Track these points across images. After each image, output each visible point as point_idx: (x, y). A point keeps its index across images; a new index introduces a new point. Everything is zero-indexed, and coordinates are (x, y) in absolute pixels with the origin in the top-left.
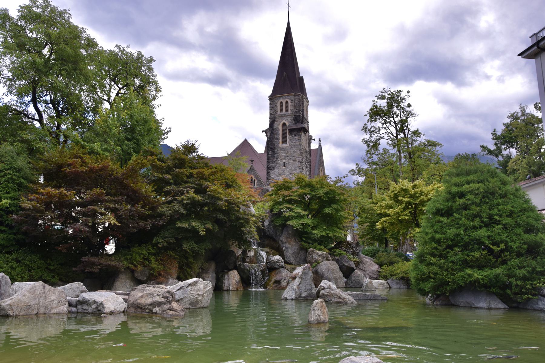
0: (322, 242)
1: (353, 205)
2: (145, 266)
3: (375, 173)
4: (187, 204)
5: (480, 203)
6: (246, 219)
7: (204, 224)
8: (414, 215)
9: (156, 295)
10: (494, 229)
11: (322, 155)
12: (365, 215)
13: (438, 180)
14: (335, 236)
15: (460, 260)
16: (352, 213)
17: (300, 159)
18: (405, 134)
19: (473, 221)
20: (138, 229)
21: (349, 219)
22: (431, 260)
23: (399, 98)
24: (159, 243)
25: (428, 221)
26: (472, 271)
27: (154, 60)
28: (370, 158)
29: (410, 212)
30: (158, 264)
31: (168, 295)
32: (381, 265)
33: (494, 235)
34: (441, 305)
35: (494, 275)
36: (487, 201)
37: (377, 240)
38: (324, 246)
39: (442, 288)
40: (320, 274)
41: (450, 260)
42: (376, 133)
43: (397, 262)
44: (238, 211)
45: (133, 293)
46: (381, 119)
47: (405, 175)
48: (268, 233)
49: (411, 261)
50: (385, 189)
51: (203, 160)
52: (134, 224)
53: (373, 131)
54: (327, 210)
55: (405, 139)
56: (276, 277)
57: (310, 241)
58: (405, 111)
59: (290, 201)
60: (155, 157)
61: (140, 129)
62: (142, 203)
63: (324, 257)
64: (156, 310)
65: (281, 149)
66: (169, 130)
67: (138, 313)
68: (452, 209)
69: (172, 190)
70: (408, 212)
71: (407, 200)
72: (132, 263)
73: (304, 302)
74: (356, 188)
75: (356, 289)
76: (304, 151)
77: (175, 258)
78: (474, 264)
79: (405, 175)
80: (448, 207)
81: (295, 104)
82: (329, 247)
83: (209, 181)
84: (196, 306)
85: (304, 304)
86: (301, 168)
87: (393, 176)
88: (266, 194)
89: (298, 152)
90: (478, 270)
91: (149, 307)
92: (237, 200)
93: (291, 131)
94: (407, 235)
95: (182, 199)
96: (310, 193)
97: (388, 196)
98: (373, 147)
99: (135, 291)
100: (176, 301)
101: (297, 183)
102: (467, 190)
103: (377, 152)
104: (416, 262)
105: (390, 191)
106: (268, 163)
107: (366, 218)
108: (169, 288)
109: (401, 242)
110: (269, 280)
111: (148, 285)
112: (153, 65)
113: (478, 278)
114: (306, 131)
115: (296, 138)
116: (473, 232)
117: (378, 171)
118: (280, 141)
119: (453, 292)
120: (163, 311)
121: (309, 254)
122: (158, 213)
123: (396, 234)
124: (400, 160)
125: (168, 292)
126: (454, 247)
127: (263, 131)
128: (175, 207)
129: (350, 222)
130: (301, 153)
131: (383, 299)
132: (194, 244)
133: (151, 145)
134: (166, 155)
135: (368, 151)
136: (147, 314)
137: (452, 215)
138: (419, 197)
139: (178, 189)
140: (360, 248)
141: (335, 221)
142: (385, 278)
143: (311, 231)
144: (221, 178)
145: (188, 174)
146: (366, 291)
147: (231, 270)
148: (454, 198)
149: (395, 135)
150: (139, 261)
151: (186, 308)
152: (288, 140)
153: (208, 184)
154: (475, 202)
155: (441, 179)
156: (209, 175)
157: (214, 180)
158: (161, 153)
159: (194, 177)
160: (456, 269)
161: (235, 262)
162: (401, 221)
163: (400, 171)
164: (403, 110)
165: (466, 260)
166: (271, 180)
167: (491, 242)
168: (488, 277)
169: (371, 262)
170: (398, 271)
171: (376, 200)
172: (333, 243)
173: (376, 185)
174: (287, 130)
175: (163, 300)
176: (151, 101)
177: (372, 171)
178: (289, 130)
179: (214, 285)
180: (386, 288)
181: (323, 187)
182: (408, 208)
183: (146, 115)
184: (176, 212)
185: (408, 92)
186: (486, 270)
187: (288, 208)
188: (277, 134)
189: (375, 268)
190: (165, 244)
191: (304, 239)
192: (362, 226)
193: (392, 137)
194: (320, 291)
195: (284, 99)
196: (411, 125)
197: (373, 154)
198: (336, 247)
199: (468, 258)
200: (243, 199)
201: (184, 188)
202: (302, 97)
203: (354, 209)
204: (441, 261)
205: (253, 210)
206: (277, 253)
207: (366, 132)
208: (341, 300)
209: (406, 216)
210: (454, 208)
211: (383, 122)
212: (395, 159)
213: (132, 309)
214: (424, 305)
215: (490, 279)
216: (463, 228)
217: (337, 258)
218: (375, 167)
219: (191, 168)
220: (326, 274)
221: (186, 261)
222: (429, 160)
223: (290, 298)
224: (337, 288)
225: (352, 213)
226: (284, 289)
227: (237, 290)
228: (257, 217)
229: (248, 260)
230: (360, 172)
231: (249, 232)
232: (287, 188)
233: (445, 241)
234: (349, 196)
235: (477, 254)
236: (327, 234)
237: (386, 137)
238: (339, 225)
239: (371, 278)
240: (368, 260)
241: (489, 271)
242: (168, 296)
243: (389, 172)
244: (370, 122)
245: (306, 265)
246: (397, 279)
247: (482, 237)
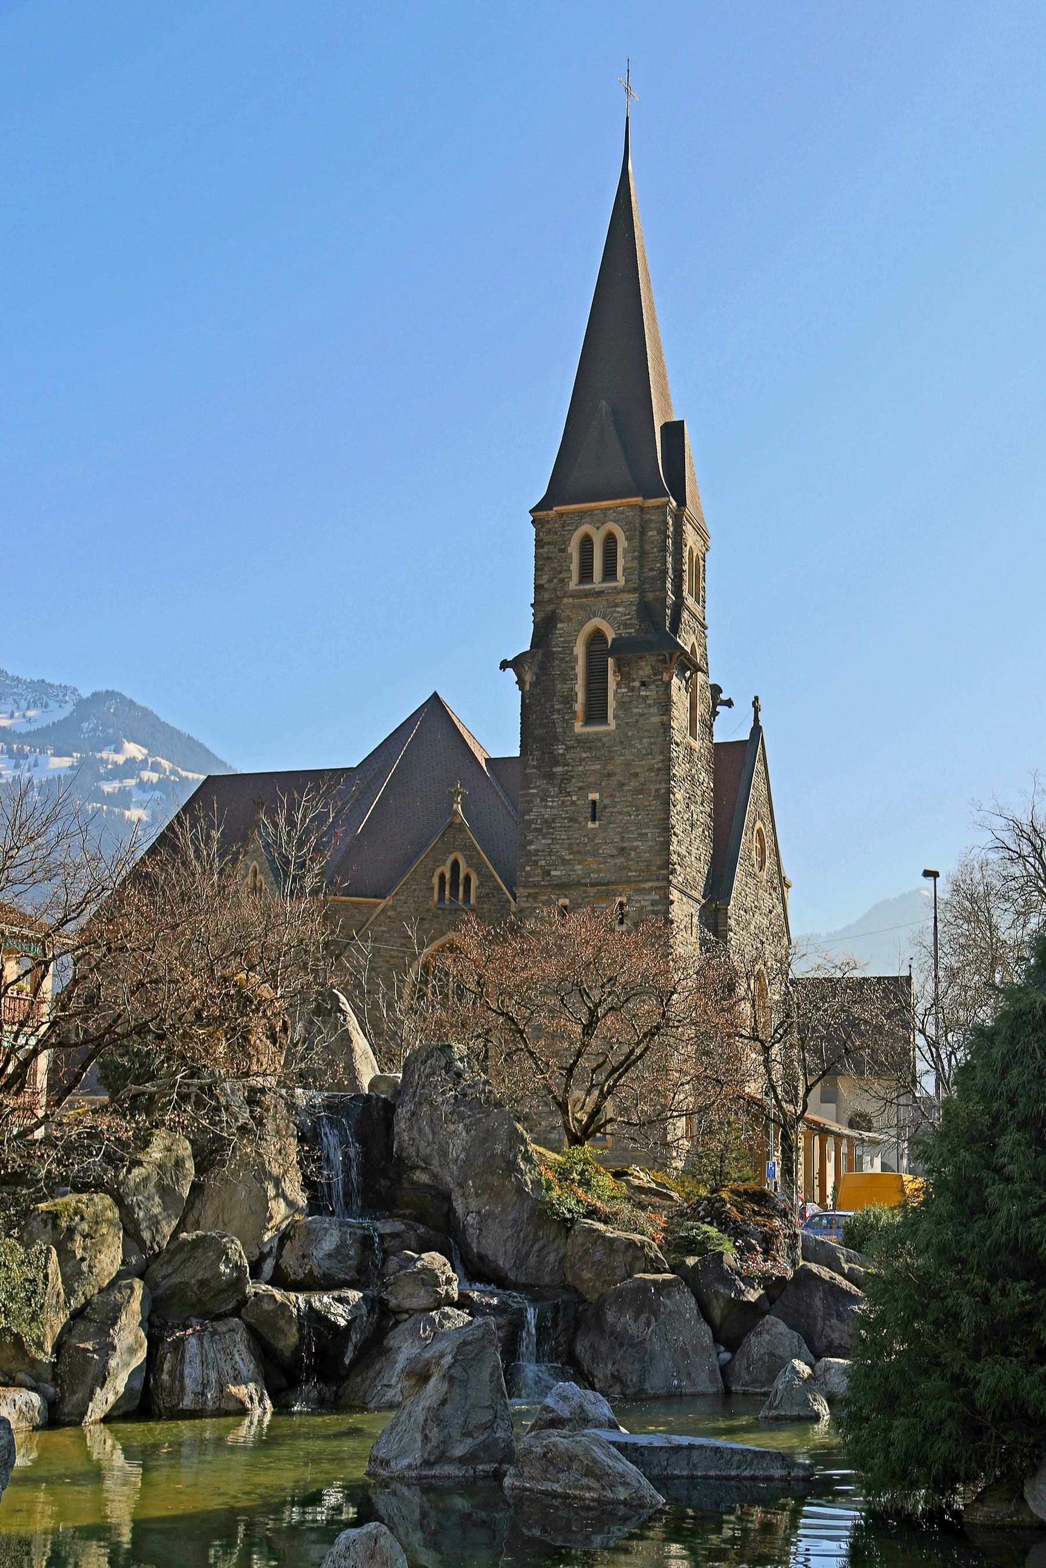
127: (504, 665)
195: (599, 524)
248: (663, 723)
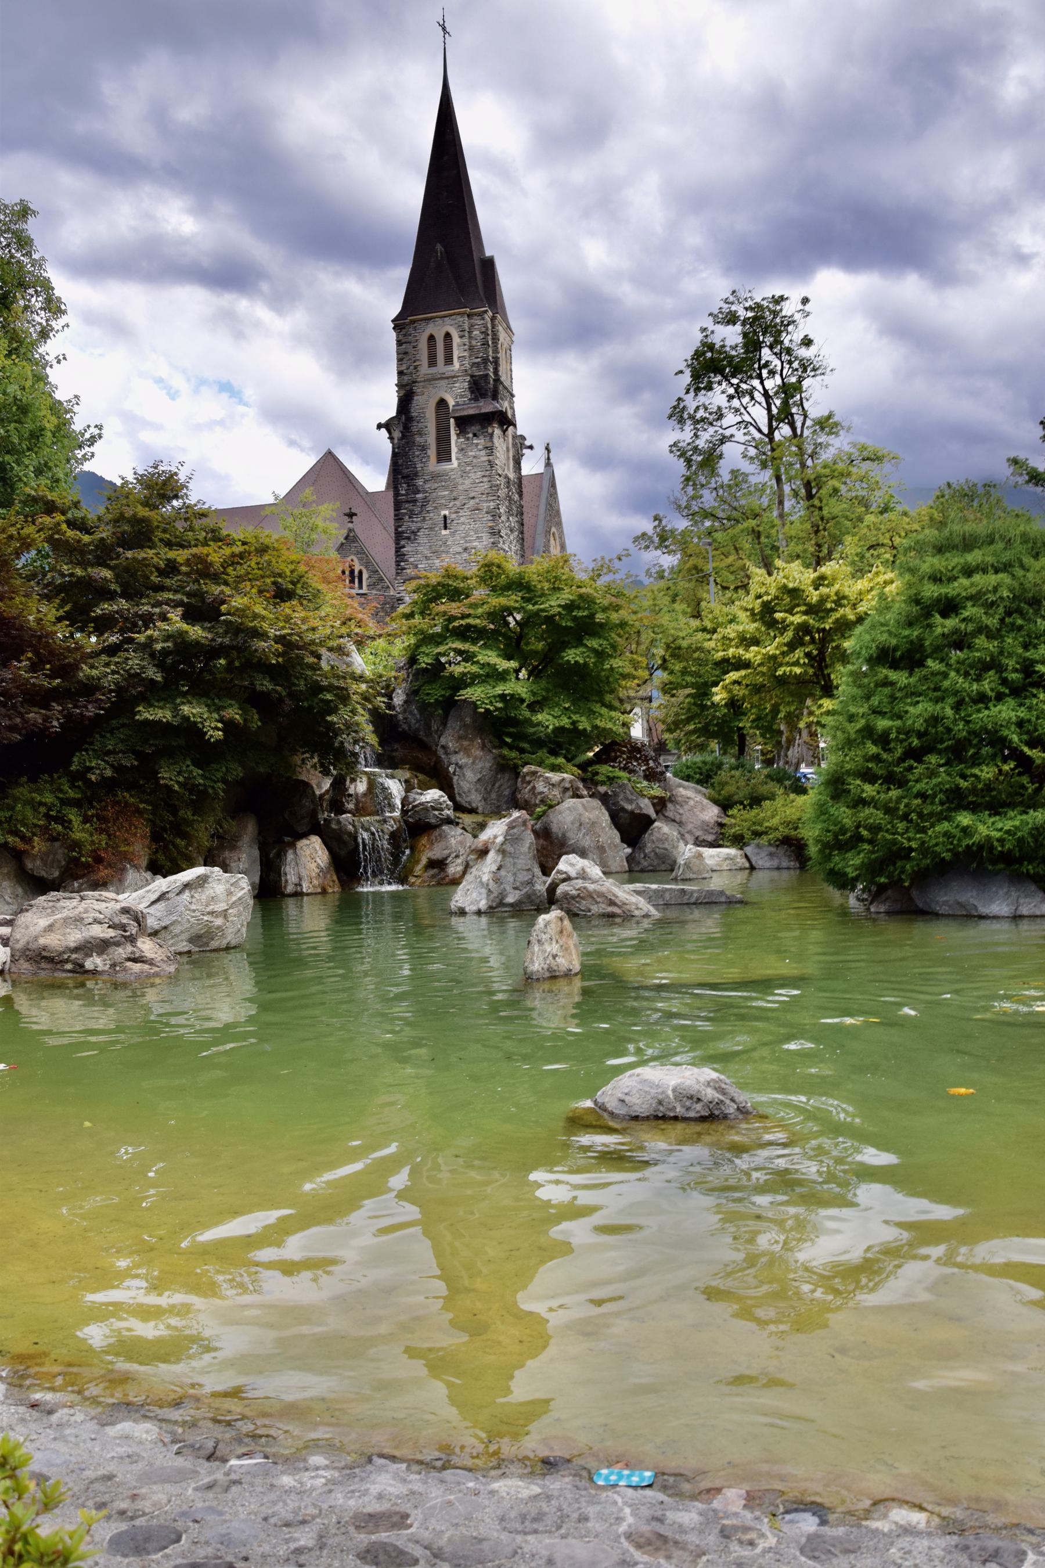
0: (559, 745)
1: (646, 637)
2: (53, 839)
3: (710, 544)
4: (165, 652)
5: (999, 630)
6: (338, 688)
7: (218, 709)
8: (820, 663)
9: (91, 920)
10: (1035, 701)
11: (556, 493)
12: (682, 665)
13: (887, 561)
14: (596, 727)
15: (941, 790)
16: (643, 661)
17: (492, 505)
18: (793, 428)
19: (978, 679)
20: (23, 732)
21: (634, 678)
22: (863, 791)
23: (778, 320)
24: (90, 769)
25: (854, 682)
26: (974, 817)
27: (34, 212)
28: (693, 498)
29: (808, 655)
30: (91, 829)
31: (124, 919)
32: (725, 805)
33: (1033, 719)
34: (888, 913)
35: (1032, 829)
36: (1020, 622)
37: (713, 735)
38: (565, 758)
39: (891, 868)
40: (557, 838)
41: (915, 790)
42: (711, 424)
43: (772, 797)
44: (315, 668)
45: (24, 919)
46: (724, 384)
47: (795, 548)
48: (405, 727)
49: (810, 792)
50: (736, 588)
51: (204, 521)
52: (10, 719)
53: (703, 420)
54: (573, 655)
55: (795, 441)
56: (432, 850)
57: (526, 746)
58: (796, 358)
59: (464, 633)
60: (59, 517)
61: (7, 431)
62: (30, 655)
63: (566, 790)
64: (95, 962)
65: (436, 477)
66: (96, 431)
67: (43, 974)
68: (922, 646)
69: (117, 612)
70: (802, 655)
71: (798, 619)
72: (16, 833)
73: (513, 917)
74: (655, 588)
75: (658, 874)
76: (502, 481)
77: (139, 812)
78: (979, 800)
79: (795, 548)
80: (912, 642)
81: (474, 343)
82: (581, 758)
83: (226, 584)
84: (207, 944)
85: (513, 924)
86: (495, 533)
87: (762, 551)
88: (393, 615)
89: (486, 485)
90: (990, 816)
91: (74, 956)
92: (310, 636)
93: (464, 423)
94: (799, 717)
95: (150, 637)
96: (523, 608)
97: (747, 610)
98: (702, 465)
99: (28, 914)
100: (150, 935)
101: (483, 580)
102: (964, 594)
103: (713, 481)
104: (824, 798)
105: (753, 593)
106: (398, 519)
107: (684, 672)
108: (129, 898)
109: (784, 739)
110: (414, 859)
111: (67, 895)
112: (32, 227)
113: (988, 838)
114: (505, 421)
115: (477, 444)
116: (979, 711)
117: (719, 536)
118: (432, 452)
119: (924, 878)
120: (113, 965)
121: (523, 782)
122: (80, 682)
123: (769, 718)
124: (781, 503)
125: (125, 911)
126: (926, 754)
127: (379, 426)
128: (130, 662)
129: (639, 685)
130: (494, 488)
131: (731, 902)
132: (192, 767)
133: (44, 481)
134: (93, 510)
135: (688, 479)
136: (70, 975)
137: (921, 664)
138: (832, 610)
139: (136, 609)
140: (670, 758)
141: (595, 687)
142: (738, 841)
143: (527, 714)
144: (261, 572)
145: (162, 565)
146: (685, 880)
147: (305, 835)
148: (928, 615)
149: (766, 430)
150: (36, 826)
151: (180, 954)
152: (454, 449)
153: (222, 592)
154: (987, 626)
155: (895, 556)
156: (225, 565)
157: (240, 579)
158: (76, 505)
159: (179, 573)
160: (931, 815)
161: (314, 814)
162: (782, 681)
163: (781, 536)
164: (790, 355)
165: (958, 788)
166: (410, 572)
167: (1025, 737)
168: (1015, 834)
169: (699, 798)
170: (775, 822)
171: (712, 621)
172: (590, 749)
173: (712, 579)
174: (452, 421)
175: (111, 933)
176: (34, 344)
177: (699, 538)
178: (457, 419)
179: (257, 880)
180: (741, 869)
181: (559, 589)
182: (803, 644)
183: (23, 389)
184: (134, 677)
185: (805, 301)
186: (1011, 814)
187: (459, 652)
188: (420, 433)
189: (711, 814)
190: (109, 773)
191: (508, 740)
192: (673, 696)
193: (757, 435)
194: (557, 885)
196: (811, 401)
197: (702, 486)
198: (599, 759)
199: (964, 784)
200: (328, 631)
201: (153, 606)
202: (493, 319)
203: (648, 649)
204: (891, 793)
205: (359, 662)
206: (433, 782)
207: (681, 421)
209: (796, 665)
210: (927, 643)
211: (731, 391)
212: (765, 501)
213: (25, 966)
214: (844, 912)
215: (1021, 840)
216: (951, 700)
217: (602, 789)
218: (708, 523)
219: (169, 544)
220: (574, 837)
221: (171, 818)
222: (865, 503)
223: (474, 908)
224: (604, 873)
225: (643, 661)
226: (456, 882)
227: (324, 892)
228: (372, 681)
229: (351, 806)
230: (666, 540)
231: (351, 727)
232: (455, 594)
233: (902, 736)
234: (635, 613)
235: (986, 773)
236: (574, 723)
237: (740, 436)
238: (608, 698)
239: (699, 842)
240: (689, 793)
241: (1019, 817)
242: (125, 921)
243: (750, 538)
244: (692, 394)
245: (516, 814)
246: (770, 845)
247: (1001, 726)
248: (490, 461)
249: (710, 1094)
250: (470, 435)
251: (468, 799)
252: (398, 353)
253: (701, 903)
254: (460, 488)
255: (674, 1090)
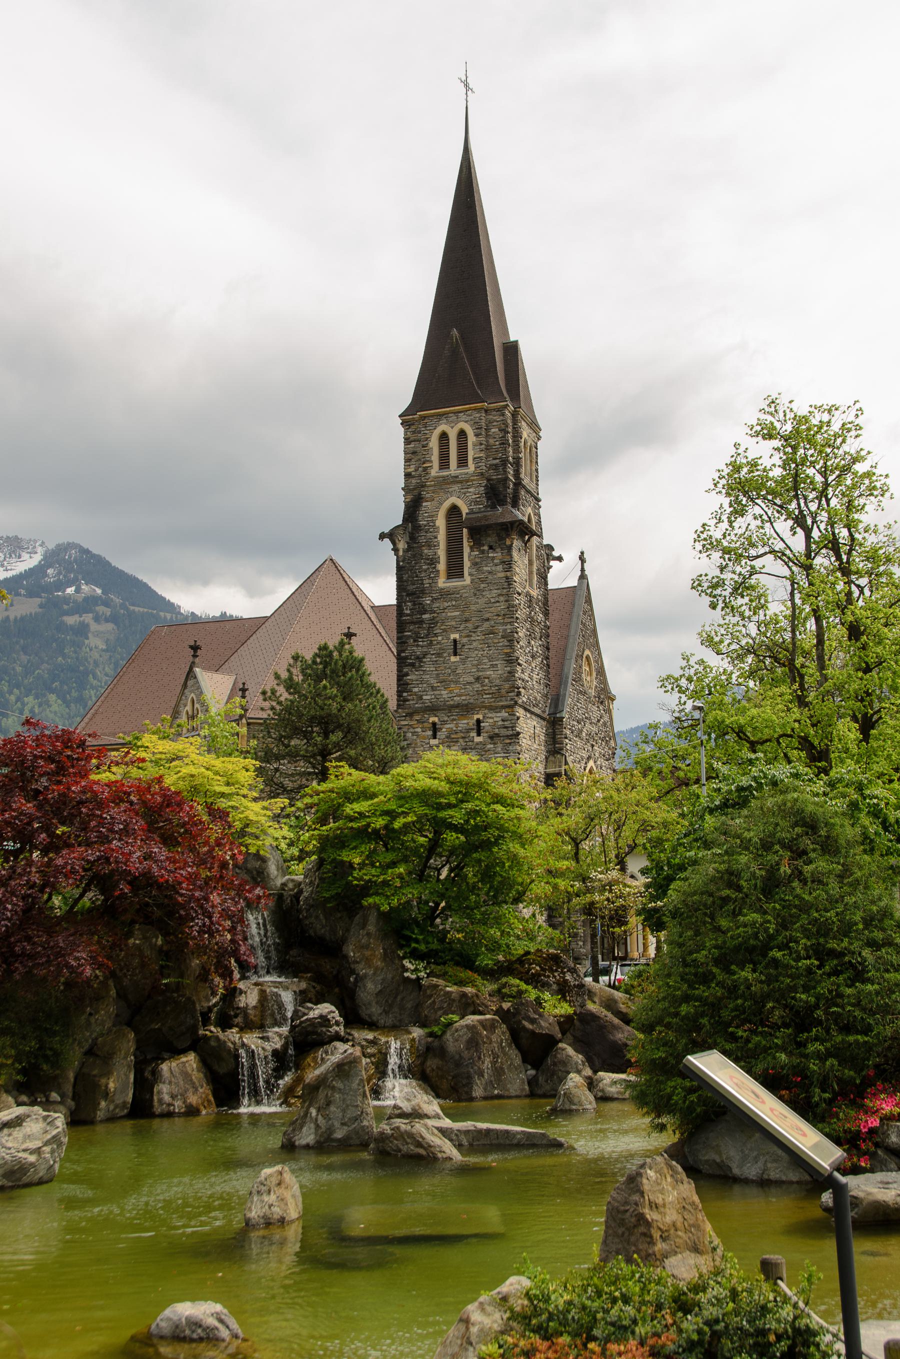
65: (445, 594)
81: (491, 441)
84: (20, 1179)
89: (503, 606)
93: (478, 532)
106: (401, 643)
115: (493, 558)
118: (442, 566)
127: (382, 536)
152: (467, 563)
174: (465, 530)
195: (452, 424)
202: (514, 415)
208: (422, 1151)
248: (507, 578)
249: (212, 1322)
250: (486, 548)
251: (368, 1012)
252: (406, 453)
253: (523, 1145)
254: (473, 608)
255: (186, 1318)
